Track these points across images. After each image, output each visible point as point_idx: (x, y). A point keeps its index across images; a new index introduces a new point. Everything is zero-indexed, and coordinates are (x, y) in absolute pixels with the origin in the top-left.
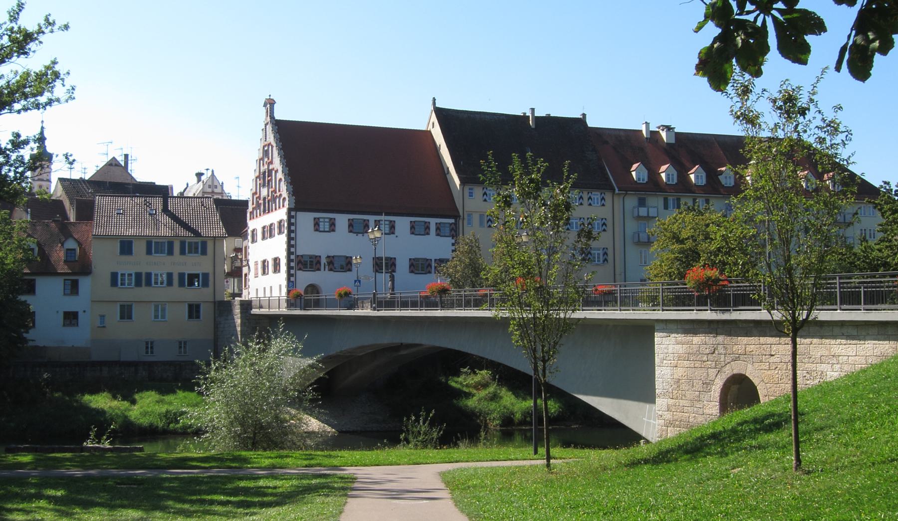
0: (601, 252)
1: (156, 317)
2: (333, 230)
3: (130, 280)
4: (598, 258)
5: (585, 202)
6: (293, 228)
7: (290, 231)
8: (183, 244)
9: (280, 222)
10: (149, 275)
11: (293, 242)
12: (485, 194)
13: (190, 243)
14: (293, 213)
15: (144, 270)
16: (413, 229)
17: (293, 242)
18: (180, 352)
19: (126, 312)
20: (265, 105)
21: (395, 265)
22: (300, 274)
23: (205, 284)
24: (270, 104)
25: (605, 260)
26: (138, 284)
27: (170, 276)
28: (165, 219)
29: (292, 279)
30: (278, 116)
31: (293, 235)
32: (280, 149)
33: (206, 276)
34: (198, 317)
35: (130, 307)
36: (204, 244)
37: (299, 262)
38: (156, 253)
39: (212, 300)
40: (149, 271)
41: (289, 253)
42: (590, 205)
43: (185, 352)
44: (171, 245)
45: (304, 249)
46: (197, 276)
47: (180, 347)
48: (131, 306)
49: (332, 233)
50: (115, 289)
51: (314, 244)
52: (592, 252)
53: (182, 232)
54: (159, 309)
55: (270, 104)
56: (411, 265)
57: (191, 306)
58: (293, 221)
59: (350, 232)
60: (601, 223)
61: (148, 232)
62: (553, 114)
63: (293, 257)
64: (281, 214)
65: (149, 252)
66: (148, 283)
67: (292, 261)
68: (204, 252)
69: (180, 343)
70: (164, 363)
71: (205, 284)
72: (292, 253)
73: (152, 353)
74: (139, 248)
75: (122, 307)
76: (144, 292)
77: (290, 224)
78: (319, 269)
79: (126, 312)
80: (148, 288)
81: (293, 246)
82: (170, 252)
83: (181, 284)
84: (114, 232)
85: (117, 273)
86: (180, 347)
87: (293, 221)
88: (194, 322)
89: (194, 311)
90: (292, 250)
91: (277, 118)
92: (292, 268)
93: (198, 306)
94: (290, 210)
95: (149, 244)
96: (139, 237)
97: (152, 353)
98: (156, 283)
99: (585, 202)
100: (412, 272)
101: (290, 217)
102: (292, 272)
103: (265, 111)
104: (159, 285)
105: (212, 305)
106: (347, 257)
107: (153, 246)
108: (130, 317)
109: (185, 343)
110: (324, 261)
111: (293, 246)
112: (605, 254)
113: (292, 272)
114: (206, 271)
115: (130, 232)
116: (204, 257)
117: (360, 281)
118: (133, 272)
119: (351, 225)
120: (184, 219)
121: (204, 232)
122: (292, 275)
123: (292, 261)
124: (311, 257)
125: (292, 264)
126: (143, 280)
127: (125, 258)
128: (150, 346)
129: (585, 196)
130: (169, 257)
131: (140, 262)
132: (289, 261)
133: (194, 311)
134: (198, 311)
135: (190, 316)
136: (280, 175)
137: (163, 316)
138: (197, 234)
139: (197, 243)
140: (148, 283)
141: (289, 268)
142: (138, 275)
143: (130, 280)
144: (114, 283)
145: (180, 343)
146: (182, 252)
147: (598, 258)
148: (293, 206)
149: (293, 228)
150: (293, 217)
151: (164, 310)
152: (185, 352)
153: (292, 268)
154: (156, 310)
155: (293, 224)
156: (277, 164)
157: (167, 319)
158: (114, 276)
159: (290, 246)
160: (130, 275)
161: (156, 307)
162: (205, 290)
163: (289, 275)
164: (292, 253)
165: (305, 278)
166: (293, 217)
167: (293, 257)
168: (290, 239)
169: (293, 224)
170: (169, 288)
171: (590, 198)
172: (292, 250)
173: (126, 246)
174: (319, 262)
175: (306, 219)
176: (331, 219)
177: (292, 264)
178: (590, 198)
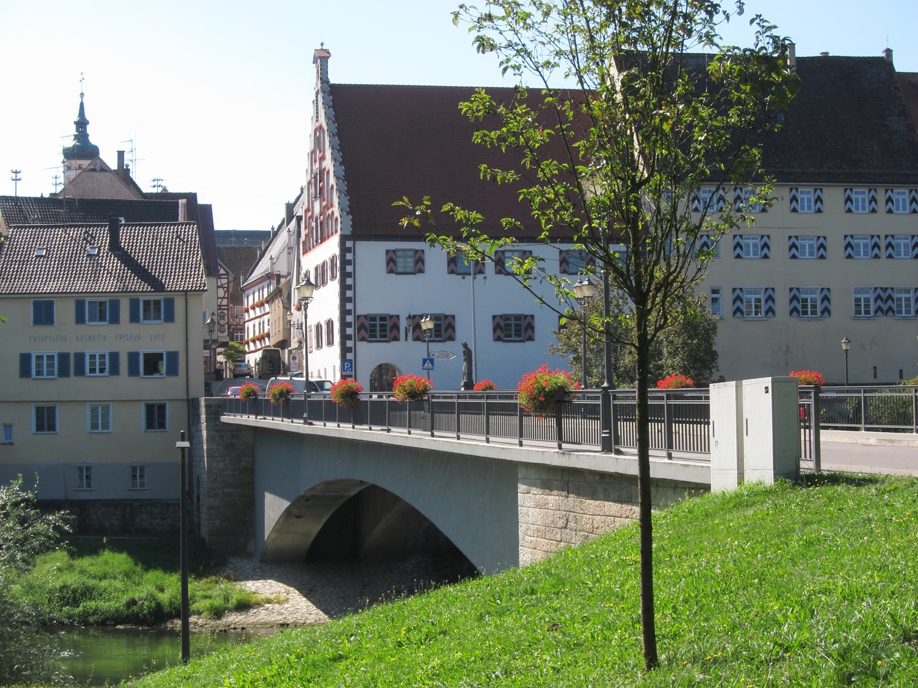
0: (818, 297)
1: (94, 426)
2: (421, 271)
3: (51, 365)
4: (908, 306)
5: (881, 206)
6: (349, 269)
7: (344, 275)
8: (134, 304)
9: (333, 260)
10: (80, 357)
11: (349, 294)
12: (849, 199)
13: (147, 303)
14: (349, 244)
15: (72, 348)
16: (392, 263)
17: (349, 294)
18: (134, 485)
19: (46, 419)
20: (315, 62)
21: (533, 328)
22: (362, 347)
23: (173, 370)
24: (322, 59)
25: (770, 310)
26: (64, 372)
27: (114, 357)
28: (113, 263)
29: (350, 356)
30: (336, 78)
31: (349, 281)
32: (332, 135)
33: (173, 357)
34: (162, 425)
35: (51, 411)
36: (170, 303)
37: (362, 327)
38: (90, 320)
39: (185, 398)
40: (80, 351)
41: (344, 312)
42: (890, 211)
43: (142, 485)
44: (115, 305)
45: (366, 306)
46: (159, 356)
47: (134, 477)
48: (54, 408)
49: (419, 275)
50: (26, 381)
51: (383, 294)
52: (896, 296)
53: (136, 284)
54: (99, 415)
55: (322, 59)
56: (496, 327)
57: (150, 408)
58: (349, 256)
59: (451, 272)
60: (871, 243)
61: (79, 286)
62: (835, 51)
63: (350, 319)
64: (331, 248)
65: (80, 319)
66: (80, 371)
67: (349, 325)
68: (170, 318)
69: (134, 469)
70: (106, 503)
71: (173, 370)
72: (349, 312)
73: (89, 485)
74: (64, 312)
75: (39, 410)
76: (72, 387)
77: (345, 262)
78: (396, 339)
79: (46, 419)
80: (80, 379)
81: (349, 300)
82: (115, 320)
83: (133, 371)
84: (25, 286)
85: (68, 355)
86: (134, 477)
87: (349, 256)
88: (156, 435)
89: (155, 415)
90: (349, 306)
91: (332, 82)
92: (349, 337)
93: (162, 408)
94: (343, 239)
95: (80, 305)
96: (63, 295)
97: (89, 485)
98: (92, 370)
99: (881, 206)
100: (498, 339)
101: (344, 250)
102: (349, 344)
103: (315, 71)
104: (98, 373)
105: (185, 405)
106: (446, 317)
107: (104, 310)
108: (52, 427)
109: (142, 469)
110: (403, 324)
111: (349, 300)
112: (770, 298)
113: (349, 344)
114: (172, 349)
115: (51, 287)
116: (169, 325)
117: (432, 361)
118: (106, 351)
119: (564, 261)
120: (143, 262)
121: (170, 284)
122: (349, 350)
123: (349, 325)
124: (518, 317)
125: (350, 331)
126: (69, 365)
127: (43, 330)
128: (86, 473)
129: (881, 196)
130: (114, 327)
131: (67, 335)
132: (344, 325)
133: (155, 415)
134: (162, 417)
135: (150, 425)
136: (332, 181)
137: (106, 426)
138: (158, 285)
139: (157, 303)
140: (80, 371)
141: (344, 337)
142: (64, 357)
143: (51, 365)
144: (25, 371)
145: (134, 469)
146: (134, 318)
147: (908, 306)
148: (348, 231)
149: (349, 269)
150: (349, 250)
151: (106, 415)
152: (142, 485)
153: (349, 337)
154: (94, 417)
155: (349, 262)
156: (328, 164)
157: (111, 430)
158: (25, 359)
159: (344, 300)
160: (51, 358)
161: (94, 410)
162: (171, 380)
163: (344, 350)
164: (349, 312)
165: (372, 354)
166: (349, 250)
167: (350, 319)
168: (344, 288)
169: (349, 262)
170: (115, 378)
171: (889, 200)
172: (349, 306)
173: (44, 311)
174: (396, 327)
175: (372, 254)
176: (417, 251)
177: (350, 331)
178: (889, 200)
